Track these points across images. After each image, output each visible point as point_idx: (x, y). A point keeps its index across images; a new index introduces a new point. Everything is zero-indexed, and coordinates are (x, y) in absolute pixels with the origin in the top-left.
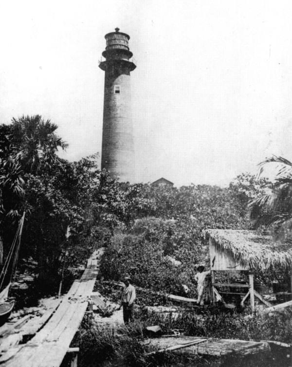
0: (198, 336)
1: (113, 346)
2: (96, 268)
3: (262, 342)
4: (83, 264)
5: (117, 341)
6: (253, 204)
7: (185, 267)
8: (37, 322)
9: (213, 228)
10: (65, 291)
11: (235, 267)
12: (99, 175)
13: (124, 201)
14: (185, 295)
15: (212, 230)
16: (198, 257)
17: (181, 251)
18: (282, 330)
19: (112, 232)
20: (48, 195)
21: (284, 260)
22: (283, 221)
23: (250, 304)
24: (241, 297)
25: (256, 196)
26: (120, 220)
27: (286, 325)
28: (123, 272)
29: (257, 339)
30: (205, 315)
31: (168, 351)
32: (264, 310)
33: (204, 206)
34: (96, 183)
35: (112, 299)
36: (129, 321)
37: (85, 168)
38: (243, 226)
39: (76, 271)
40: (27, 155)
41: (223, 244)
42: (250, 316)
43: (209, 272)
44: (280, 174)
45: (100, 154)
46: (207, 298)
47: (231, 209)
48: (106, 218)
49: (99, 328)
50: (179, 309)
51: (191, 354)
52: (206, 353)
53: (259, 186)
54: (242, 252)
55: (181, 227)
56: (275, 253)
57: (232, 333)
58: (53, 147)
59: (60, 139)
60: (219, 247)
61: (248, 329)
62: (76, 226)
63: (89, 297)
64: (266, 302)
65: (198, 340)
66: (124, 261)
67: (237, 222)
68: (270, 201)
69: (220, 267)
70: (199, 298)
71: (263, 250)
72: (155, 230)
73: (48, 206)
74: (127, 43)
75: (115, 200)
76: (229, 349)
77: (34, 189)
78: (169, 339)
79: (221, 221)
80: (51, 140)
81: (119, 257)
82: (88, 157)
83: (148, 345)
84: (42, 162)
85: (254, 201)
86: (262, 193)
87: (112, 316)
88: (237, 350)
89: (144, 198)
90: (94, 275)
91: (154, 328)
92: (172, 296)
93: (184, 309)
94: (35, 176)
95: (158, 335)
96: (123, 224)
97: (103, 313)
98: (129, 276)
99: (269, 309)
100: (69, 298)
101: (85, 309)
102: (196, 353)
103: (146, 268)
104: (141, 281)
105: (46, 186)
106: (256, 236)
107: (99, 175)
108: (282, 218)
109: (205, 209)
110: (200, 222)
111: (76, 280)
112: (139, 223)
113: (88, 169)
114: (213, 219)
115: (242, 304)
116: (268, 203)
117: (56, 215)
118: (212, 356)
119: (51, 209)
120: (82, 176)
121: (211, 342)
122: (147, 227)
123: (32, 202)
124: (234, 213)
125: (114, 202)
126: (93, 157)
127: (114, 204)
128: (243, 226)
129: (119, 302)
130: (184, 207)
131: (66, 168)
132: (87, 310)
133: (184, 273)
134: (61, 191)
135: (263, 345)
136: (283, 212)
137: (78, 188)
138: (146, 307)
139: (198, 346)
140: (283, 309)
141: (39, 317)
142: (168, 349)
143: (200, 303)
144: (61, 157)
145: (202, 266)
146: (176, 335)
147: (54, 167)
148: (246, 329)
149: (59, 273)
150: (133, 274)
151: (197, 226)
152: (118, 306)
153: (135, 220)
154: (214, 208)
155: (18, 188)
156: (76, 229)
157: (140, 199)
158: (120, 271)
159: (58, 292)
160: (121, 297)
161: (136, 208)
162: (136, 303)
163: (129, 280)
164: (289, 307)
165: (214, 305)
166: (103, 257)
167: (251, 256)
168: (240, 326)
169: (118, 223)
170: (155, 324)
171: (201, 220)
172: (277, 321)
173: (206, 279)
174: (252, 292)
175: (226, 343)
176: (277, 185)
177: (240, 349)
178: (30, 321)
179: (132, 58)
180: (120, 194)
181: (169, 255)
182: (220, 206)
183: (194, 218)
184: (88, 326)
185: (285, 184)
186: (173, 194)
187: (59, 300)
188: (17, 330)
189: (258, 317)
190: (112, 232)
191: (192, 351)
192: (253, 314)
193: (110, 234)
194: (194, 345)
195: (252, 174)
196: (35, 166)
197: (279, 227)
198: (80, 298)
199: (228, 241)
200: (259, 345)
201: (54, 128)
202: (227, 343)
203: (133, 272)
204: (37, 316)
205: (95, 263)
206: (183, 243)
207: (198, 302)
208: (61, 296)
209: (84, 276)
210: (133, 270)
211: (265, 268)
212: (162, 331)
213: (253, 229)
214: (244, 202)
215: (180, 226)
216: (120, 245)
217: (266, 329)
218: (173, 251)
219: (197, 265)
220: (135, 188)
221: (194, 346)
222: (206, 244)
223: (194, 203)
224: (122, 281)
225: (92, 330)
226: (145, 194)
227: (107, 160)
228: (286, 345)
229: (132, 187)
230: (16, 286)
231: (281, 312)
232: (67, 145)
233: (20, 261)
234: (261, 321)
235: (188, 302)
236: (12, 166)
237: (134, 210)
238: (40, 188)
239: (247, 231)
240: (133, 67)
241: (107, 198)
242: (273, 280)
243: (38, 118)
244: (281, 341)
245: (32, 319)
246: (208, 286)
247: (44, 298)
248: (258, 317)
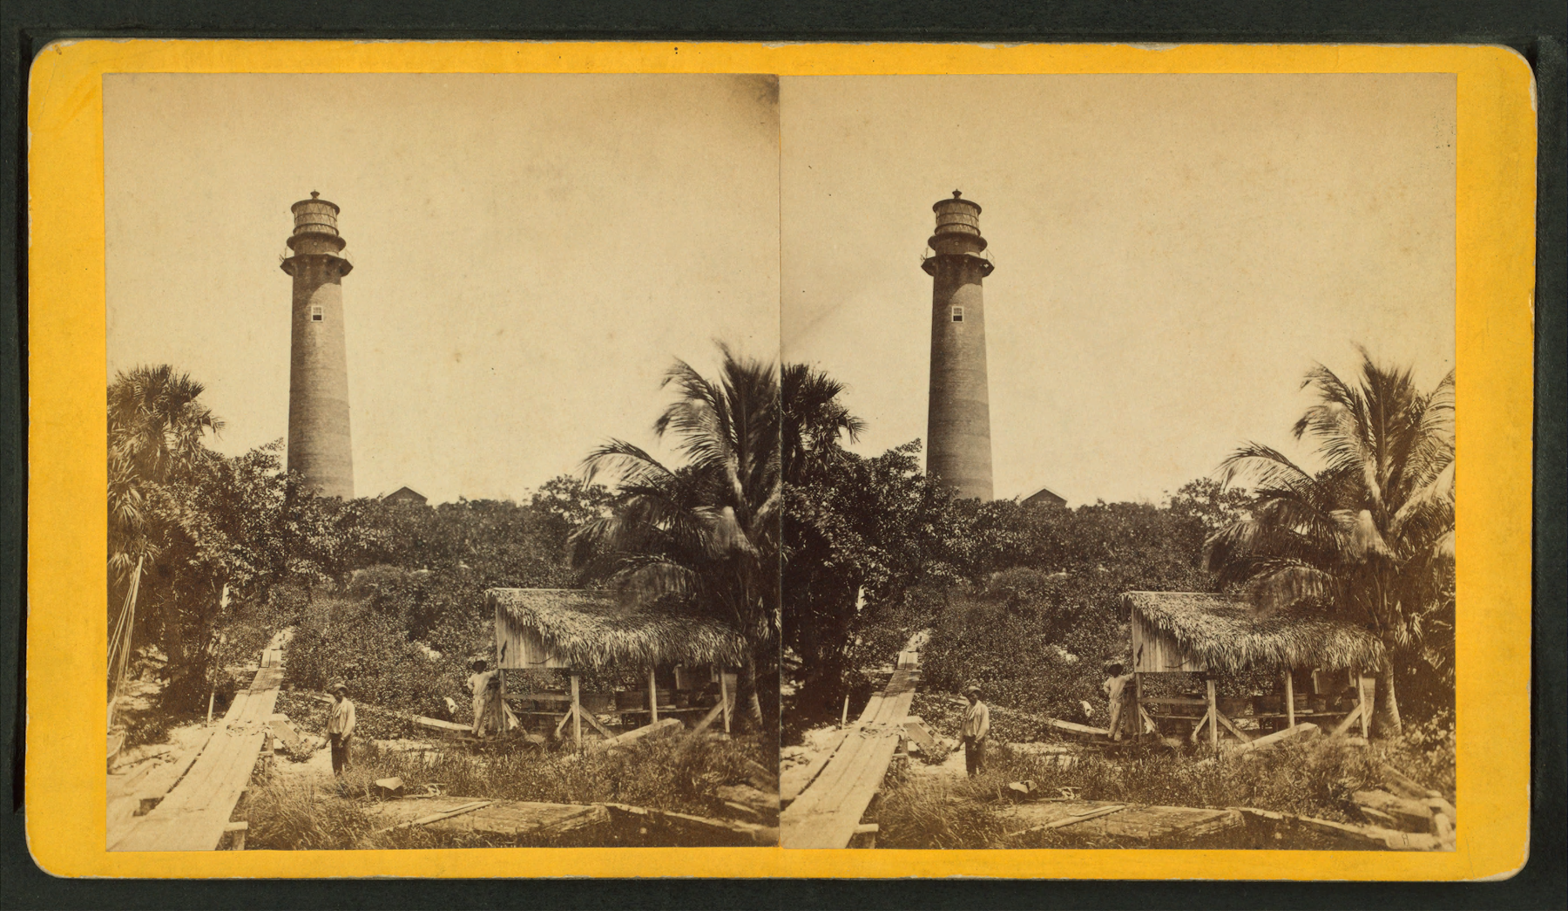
0: (474, 795)
1: (312, 817)
2: (279, 668)
3: (1229, 810)
4: (891, 661)
5: (319, 807)
6: (578, 537)
7: (1086, 667)
8: (167, 772)
9: (1139, 590)
10: (855, 713)
11: (544, 663)
12: (284, 483)
13: (968, 536)
14: (450, 718)
15: (1137, 592)
16: (473, 644)
17: (443, 630)
18: (632, 782)
19: (309, 596)
20: (185, 523)
21: (636, 645)
22: (635, 570)
23: (1209, 737)
24: (1193, 723)
25: (582, 521)
26: (324, 571)
27: (639, 771)
28: (968, 678)
29: (586, 800)
30: (487, 756)
31: (418, 825)
32: (1235, 749)
33: (485, 541)
34: (913, 501)
35: (945, 729)
36: (978, 771)
37: (257, 470)
38: (1198, 585)
39: (877, 675)
40: (145, 444)
41: (1158, 619)
42: (1207, 761)
43: (1131, 675)
44: (1265, 482)
45: (286, 442)
46: (491, 722)
47: (536, 548)
48: (297, 568)
49: (286, 783)
50: (437, 744)
51: (460, 831)
52: (490, 829)
53: (588, 502)
54: (1193, 636)
55: (441, 584)
56: (619, 634)
57: (1173, 795)
58: (196, 429)
59: (208, 412)
60: (514, 625)
61: (1203, 787)
62: (241, 583)
63: (902, 727)
64: (602, 729)
65: (474, 803)
66: (968, 655)
67: (548, 572)
68: (611, 529)
69: (517, 663)
70: (476, 724)
71: (1233, 630)
72: (1028, 593)
73: (820, 546)
74: (335, 220)
75: (952, 535)
76: (532, 822)
77: (159, 511)
78: (1053, 806)
79: (516, 572)
80: (827, 416)
81: (960, 646)
82: (897, 448)
83: (380, 816)
84: (810, 460)
85: (580, 532)
86: (594, 516)
87: (944, 763)
88: (547, 822)
89: (370, 527)
90: (911, 683)
91: (390, 783)
92: (425, 721)
93: (448, 745)
94: (796, 486)
95: (1021, 798)
96: (331, 579)
97: (927, 757)
98: (343, 682)
99: (607, 742)
100: (862, 729)
101: (893, 749)
102: (1104, 834)
103: (375, 666)
104: (1002, 694)
105: (183, 504)
106: (585, 600)
107: (284, 483)
108: (631, 564)
109: (1125, 552)
110: (1116, 577)
111: (876, 693)
112: (999, 580)
113: (262, 471)
114: (503, 567)
115: (558, 733)
116: (604, 535)
117: (202, 562)
118: (500, 834)
119: (193, 551)
120: (251, 486)
121: (498, 807)
122: (376, 585)
123: (156, 537)
124: (1179, 559)
125: (313, 535)
126: (272, 447)
127: (313, 540)
128: (1198, 585)
129: (325, 732)
130: (1085, 547)
131: (855, 471)
132: (897, 750)
133: (448, 674)
134: (211, 516)
135: (597, 811)
136: (635, 551)
137: (876, 512)
138: (376, 742)
139: (474, 816)
140: (634, 742)
141: (171, 764)
142: (418, 821)
143: (1113, 736)
144: (209, 447)
145: (482, 661)
146: (432, 794)
147: (834, 470)
148: (565, 782)
149: (207, 677)
150: (351, 678)
151: (472, 581)
152: (955, 744)
153: (352, 572)
154: (1142, 549)
155: (128, 510)
156: (241, 591)
157: (362, 531)
158: (324, 673)
159: (840, 716)
160: (327, 723)
161: (355, 547)
162: (357, 735)
163: (342, 689)
164: (645, 737)
165: (505, 736)
166: (292, 645)
167: (574, 639)
168: (554, 776)
169: (321, 579)
170: (393, 775)
171: (478, 571)
172: (622, 765)
173: (489, 686)
174: (576, 710)
175: (525, 809)
176: (623, 498)
177: (554, 820)
178: (153, 772)
179: (985, 251)
180: (959, 523)
181: (419, 640)
182: (515, 541)
183: (466, 566)
184: (266, 780)
185: (637, 497)
186: (1065, 521)
187: (209, 730)
188: (129, 790)
189: (588, 758)
190: (309, 596)
191: (462, 825)
192: (578, 751)
193: (943, 601)
194: (1100, 817)
195: (574, 478)
196: (162, 468)
197: (1265, 585)
198: (883, 728)
199: (531, 611)
200: (588, 811)
201: (833, 390)
202: (530, 810)
203: (350, 673)
204: (168, 761)
205: (278, 656)
206: (447, 616)
207: (1110, 736)
208: (846, 724)
209: (256, 682)
210: (349, 669)
211: (600, 663)
212: (405, 787)
213: (579, 587)
214: (561, 533)
215: (439, 582)
216: (961, 623)
217: (602, 781)
218: (427, 632)
219: (472, 659)
220: (352, 508)
221: (466, 816)
222: (490, 618)
223: (466, 537)
224: (328, 692)
225: (905, 791)
226: (372, 520)
227: (299, 457)
228: (640, 811)
229: (982, 508)
230: (126, 704)
231: (630, 748)
232: (222, 424)
233: (135, 656)
234: (1229, 771)
235: (456, 732)
236: (116, 466)
237: (351, 551)
238: (806, 510)
239: (1203, 594)
240: (986, 268)
241: (300, 529)
242: (1252, 689)
243: (164, 372)
244: (1265, 808)
245: (790, 769)
246: (493, 699)
247: (814, 728)
248: (588, 758)
